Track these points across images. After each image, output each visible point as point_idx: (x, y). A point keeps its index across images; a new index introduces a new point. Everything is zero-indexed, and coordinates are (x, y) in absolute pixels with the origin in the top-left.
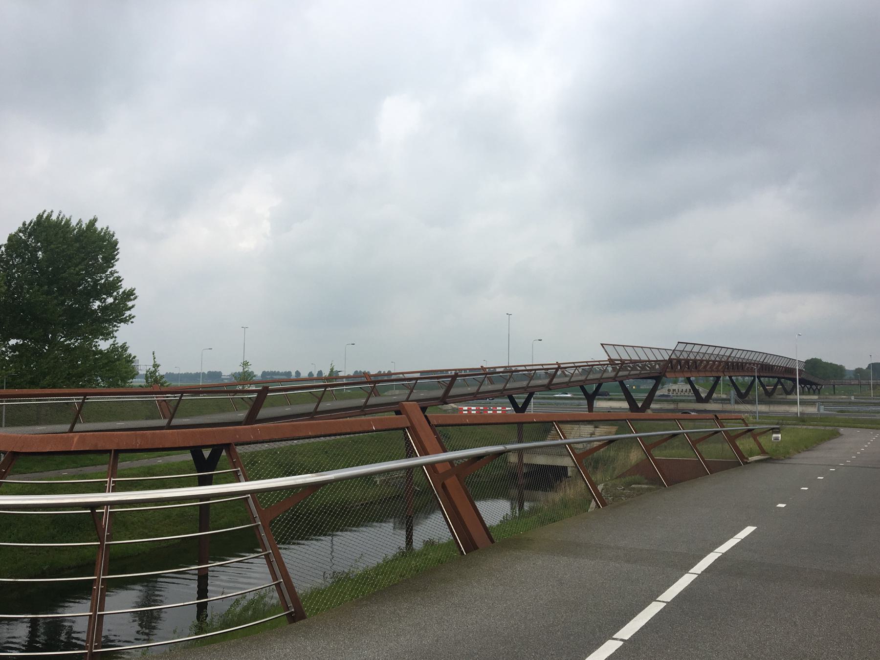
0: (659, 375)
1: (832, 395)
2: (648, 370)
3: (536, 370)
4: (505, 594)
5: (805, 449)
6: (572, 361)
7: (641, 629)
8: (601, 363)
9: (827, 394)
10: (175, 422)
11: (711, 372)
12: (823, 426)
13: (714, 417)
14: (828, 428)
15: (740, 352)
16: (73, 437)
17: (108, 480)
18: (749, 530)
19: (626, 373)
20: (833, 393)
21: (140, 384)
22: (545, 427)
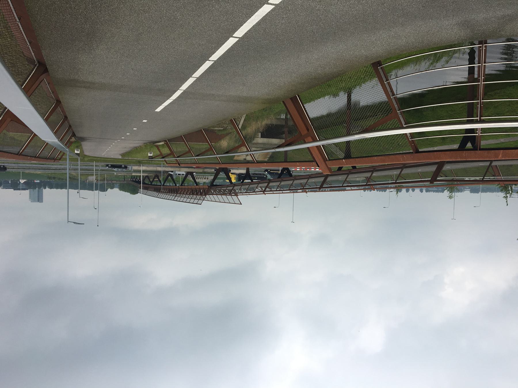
0: (212, 187)
1: (125, 175)
2: (217, 189)
3: (276, 191)
4: (270, 78)
5: (137, 148)
6: (244, 196)
7: (201, 66)
8: (242, 194)
9: (128, 176)
10: (488, 164)
11: (185, 189)
12: (130, 160)
13: (180, 164)
14: (127, 158)
15: (175, 199)
16: (502, 157)
17: (480, 134)
18: (159, 110)
19: (228, 188)
20: (125, 176)
21: (516, 186)
22: (273, 159)
